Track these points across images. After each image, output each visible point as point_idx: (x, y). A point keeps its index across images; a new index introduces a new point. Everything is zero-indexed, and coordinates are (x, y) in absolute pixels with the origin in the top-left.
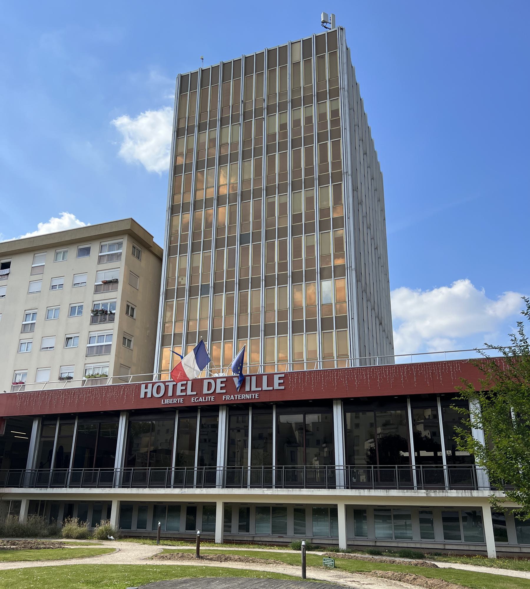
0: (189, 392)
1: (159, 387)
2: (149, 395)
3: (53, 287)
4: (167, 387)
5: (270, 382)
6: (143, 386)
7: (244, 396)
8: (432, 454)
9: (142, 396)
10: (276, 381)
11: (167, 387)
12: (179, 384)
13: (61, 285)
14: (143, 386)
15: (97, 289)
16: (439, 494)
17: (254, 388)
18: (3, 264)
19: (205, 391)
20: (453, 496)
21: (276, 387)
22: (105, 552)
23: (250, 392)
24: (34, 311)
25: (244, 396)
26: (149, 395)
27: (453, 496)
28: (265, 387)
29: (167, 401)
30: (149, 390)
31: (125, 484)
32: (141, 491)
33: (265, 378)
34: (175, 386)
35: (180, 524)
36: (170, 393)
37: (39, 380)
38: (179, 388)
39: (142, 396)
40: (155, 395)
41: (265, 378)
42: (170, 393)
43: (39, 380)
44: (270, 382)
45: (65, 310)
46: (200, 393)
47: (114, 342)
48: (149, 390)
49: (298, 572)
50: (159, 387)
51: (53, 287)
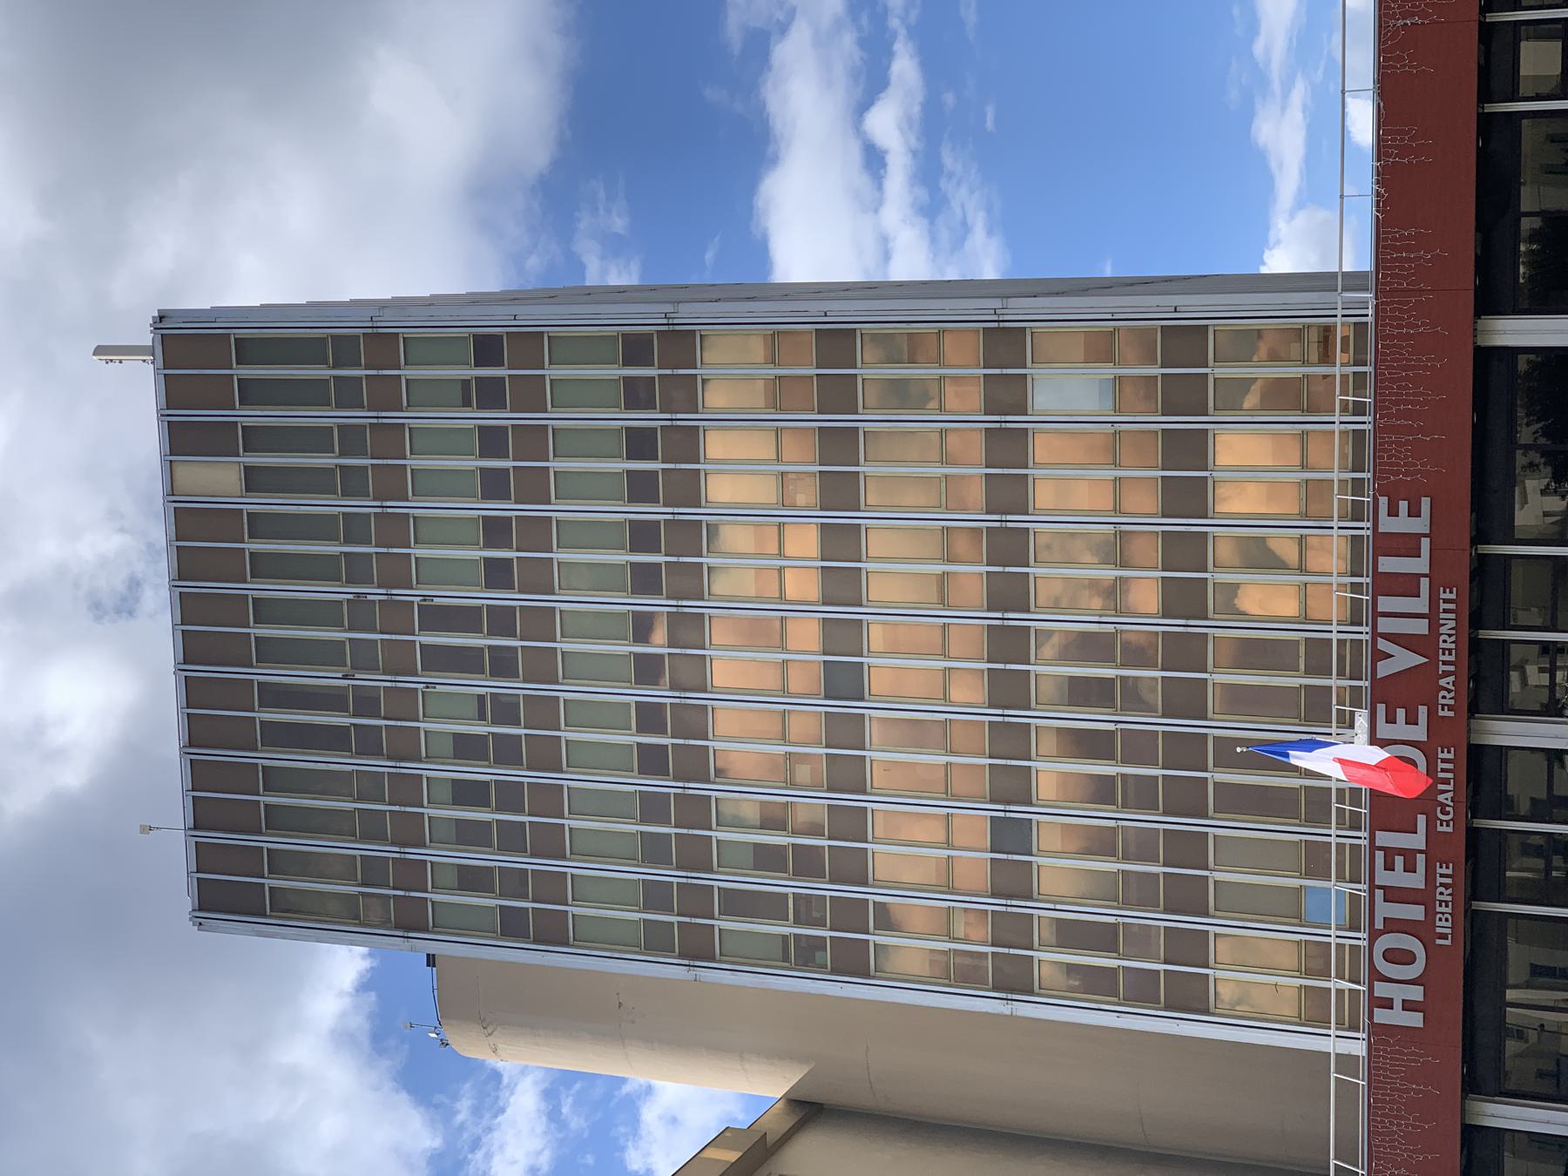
0: (1417, 841)
2: (1416, 993)
4: (1392, 925)
5: (1405, 545)
6: (1381, 1016)
9: (1415, 1020)
10: (1402, 524)
11: (1392, 925)
12: (1383, 877)
14: (1381, 1016)
17: (1420, 604)
21: (1420, 525)
23: (1432, 617)
26: (1416, 993)
28: (1420, 565)
29: (1443, 926)
30: (1398, 993)
33: (1388, 564)
34: (1394, 895)
36: (1416, 912)
39: (1415, 1020)
40: (1415, 970)
41: (1388, 564)
42: (1416, 912)
44: (1405, 545)
48: (1398, 993)
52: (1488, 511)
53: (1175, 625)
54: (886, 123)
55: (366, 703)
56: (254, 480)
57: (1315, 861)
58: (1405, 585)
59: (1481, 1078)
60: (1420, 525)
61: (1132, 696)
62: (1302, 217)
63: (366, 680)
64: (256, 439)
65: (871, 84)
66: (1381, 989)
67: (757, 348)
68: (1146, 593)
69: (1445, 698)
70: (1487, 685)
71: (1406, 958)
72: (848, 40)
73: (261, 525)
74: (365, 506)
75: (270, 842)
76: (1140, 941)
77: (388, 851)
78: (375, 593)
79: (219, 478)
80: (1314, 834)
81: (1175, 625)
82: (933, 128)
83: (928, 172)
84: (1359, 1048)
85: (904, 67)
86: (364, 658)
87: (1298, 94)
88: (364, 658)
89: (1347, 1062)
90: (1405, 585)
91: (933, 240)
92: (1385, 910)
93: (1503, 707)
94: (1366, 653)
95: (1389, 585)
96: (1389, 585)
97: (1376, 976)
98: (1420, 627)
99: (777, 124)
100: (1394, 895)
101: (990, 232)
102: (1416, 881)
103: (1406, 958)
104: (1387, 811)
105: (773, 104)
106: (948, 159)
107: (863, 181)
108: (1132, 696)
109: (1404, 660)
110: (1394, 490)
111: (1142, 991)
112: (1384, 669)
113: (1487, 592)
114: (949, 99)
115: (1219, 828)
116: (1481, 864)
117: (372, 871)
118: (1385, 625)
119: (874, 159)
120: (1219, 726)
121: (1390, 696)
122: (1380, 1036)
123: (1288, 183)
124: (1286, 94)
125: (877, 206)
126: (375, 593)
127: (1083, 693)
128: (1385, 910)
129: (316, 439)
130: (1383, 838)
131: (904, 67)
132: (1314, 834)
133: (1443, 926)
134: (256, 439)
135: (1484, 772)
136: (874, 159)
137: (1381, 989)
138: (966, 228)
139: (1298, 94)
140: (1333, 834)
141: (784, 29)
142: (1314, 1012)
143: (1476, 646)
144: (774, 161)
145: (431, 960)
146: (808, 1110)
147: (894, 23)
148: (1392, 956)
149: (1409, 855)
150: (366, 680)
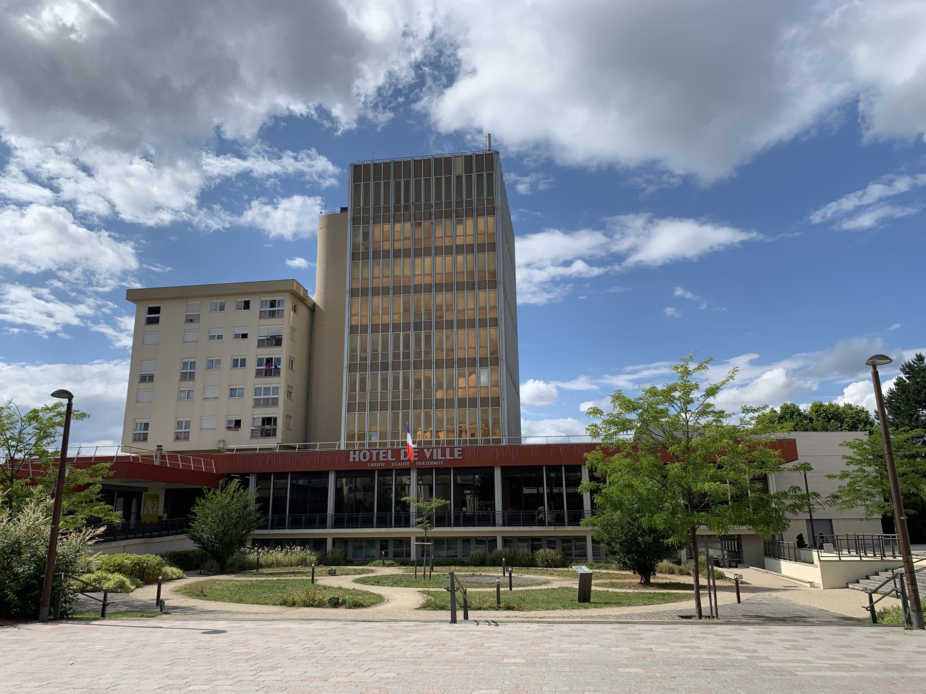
0: (390, 459)
1: (365, 454)
2: (357, 460)
3: (212, 337)
4: (371, 454)
5: (452, 454)
6: (352, 453)
7: (432, 463)
8: (534, 491)
9: (351, 460)
10: (456, 453)
11: (371, 454)
12: (381, 452)
13: (220, 337)
14: (352, 453)
15: (261, 343)
16: (562, 528)
17: (439, 457)
18: (150, 308)
19: (402, 458)
20: (569, 530)
21: (456, 457)
22: (372, 571)
23: (437, 460)
24: (193, 360)
25: (432, 463)
26: (357, 460)
27: (569, 530)
28: (448, 457)
29: (372, 465)
30: (357, 456)
31: (338, 523)
32: (355, 530)
33: (448, 451)
34: (378, 454)
35: (376, 551)
36: (374, 459)
37: (706, 584)
38: (381, 455)
39: (351, 460)
40: (362, 460)
41: (448, 451)
42: (374, 459)
43: (706, 584)
44: (452, 454)
45: (227, 363)
46: (398, 460)
47: (282, 396)
48: (357, 456)
49: (858, 559)
50: (365, 454)
51: (212, 337)
52: (459, 471)
53: (434, 402)
54: (579, 267)
55: (407, 208)
56: (459, 178)
57: (383, 435)
58: (444, 454)
59: (339, 474)
60: (456, 457)
61: (418, 393)
62: (554, 390)
63: (412, 207)
64: (469, 178)
65: (591, 261)
66: (357, 453)
67: (493, 303)
68: (440, 395)
69: (420, 463)
70: (423, 472)
71: (365, 456)
72: (603, 254)
73: (448, 180)
74: (454, 207)
75: (372, 183)
76: (363, 396)
77: (371, 215)
78: (433, 210)
79: (459, 168)
80: (389, 435)
81: (434, 402)
82: (578, 281)
83: (564, 280)
84: (342, 448)
85: (596, 271)
86: (418, 207)
87: (595, 387)
88: (418, 207)
89: (339, 446)
90: (444, 454)
91: (545, 283)
92: (374, 453)
93: (419, 475)
94: (429, 446)
95: (443, 450)
96: (443, 450)
97: (360, 451)
98: (435, 458)
99: (578, 233)
100: (378, 454)
101: (548, 299)
102: (381, 459)
103: (365, 456)
104: (396, 453)
105: (584, 232)
106: (569, 286)
107: (561, 260)
108: (418, 393)
109: (428, 454)
110: (463, 451)
111: (351, 397)
112: (426, 450)
113: (443, 471)
114: (587, 285)
115: (389, 413)
116: (385, 472)
117: (366, 211)
118: (435, 450)
119: (568, 263)
120: (411, 412)
121: (420, 452)
122: (347, 453)
123: (568, 386)
124: (595, 384)
125: (554, 264)
126: (433, 210)
127: (418, 383)
128: (374, 453)
129: (469, 194)
130: (390, 452)
131: (596, 271)
132: (389, 435)
133: (372, 465)
134: (469, 178)
135: (406, 472)
136: (568, 263)
137: (357, 453)
138: (549, 292)
139: (595, 387)
140: (389, 441)
141: (605, 235)
142: (351, 437)
143: (432, 469)
144: (566, 233)
145: (344, 210)
146: (313, 308)
147: (609, 268)
148: (365, 455)
149: (386, 457)
150: (412, 207)
